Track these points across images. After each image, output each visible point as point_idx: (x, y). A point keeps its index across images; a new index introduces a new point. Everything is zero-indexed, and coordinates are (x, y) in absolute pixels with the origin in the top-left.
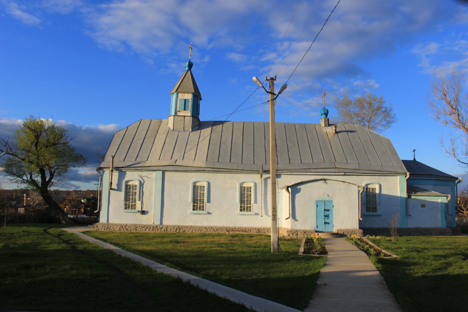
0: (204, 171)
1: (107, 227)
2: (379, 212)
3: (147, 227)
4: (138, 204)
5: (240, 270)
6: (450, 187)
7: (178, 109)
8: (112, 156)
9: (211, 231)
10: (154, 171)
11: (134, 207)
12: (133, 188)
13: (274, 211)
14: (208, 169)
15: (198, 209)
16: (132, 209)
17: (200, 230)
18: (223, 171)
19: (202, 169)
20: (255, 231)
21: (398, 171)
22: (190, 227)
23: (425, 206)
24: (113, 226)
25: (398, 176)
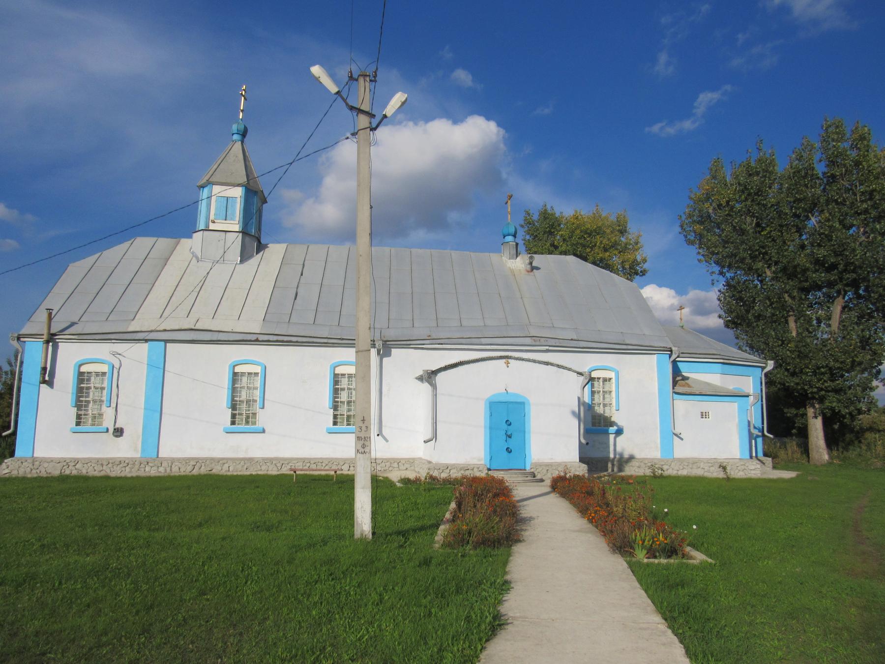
0: (257, 340)
1: (32, 468)
2: (259, 425)
3: (125, 465)
4: (108, 413)
7: (212, 217)
8: (47, 309)
9: (270, 469)
10: (146, 341)
11: (98, 417)
13: (364, 428)
14: (266, 338)
15: (244, 422)
16: (348, 425)
17: (245, 467)
19: (254, 337)
21: (656, 345)
22: (225, 461)
24: (46, 465)
25: (655, 354)
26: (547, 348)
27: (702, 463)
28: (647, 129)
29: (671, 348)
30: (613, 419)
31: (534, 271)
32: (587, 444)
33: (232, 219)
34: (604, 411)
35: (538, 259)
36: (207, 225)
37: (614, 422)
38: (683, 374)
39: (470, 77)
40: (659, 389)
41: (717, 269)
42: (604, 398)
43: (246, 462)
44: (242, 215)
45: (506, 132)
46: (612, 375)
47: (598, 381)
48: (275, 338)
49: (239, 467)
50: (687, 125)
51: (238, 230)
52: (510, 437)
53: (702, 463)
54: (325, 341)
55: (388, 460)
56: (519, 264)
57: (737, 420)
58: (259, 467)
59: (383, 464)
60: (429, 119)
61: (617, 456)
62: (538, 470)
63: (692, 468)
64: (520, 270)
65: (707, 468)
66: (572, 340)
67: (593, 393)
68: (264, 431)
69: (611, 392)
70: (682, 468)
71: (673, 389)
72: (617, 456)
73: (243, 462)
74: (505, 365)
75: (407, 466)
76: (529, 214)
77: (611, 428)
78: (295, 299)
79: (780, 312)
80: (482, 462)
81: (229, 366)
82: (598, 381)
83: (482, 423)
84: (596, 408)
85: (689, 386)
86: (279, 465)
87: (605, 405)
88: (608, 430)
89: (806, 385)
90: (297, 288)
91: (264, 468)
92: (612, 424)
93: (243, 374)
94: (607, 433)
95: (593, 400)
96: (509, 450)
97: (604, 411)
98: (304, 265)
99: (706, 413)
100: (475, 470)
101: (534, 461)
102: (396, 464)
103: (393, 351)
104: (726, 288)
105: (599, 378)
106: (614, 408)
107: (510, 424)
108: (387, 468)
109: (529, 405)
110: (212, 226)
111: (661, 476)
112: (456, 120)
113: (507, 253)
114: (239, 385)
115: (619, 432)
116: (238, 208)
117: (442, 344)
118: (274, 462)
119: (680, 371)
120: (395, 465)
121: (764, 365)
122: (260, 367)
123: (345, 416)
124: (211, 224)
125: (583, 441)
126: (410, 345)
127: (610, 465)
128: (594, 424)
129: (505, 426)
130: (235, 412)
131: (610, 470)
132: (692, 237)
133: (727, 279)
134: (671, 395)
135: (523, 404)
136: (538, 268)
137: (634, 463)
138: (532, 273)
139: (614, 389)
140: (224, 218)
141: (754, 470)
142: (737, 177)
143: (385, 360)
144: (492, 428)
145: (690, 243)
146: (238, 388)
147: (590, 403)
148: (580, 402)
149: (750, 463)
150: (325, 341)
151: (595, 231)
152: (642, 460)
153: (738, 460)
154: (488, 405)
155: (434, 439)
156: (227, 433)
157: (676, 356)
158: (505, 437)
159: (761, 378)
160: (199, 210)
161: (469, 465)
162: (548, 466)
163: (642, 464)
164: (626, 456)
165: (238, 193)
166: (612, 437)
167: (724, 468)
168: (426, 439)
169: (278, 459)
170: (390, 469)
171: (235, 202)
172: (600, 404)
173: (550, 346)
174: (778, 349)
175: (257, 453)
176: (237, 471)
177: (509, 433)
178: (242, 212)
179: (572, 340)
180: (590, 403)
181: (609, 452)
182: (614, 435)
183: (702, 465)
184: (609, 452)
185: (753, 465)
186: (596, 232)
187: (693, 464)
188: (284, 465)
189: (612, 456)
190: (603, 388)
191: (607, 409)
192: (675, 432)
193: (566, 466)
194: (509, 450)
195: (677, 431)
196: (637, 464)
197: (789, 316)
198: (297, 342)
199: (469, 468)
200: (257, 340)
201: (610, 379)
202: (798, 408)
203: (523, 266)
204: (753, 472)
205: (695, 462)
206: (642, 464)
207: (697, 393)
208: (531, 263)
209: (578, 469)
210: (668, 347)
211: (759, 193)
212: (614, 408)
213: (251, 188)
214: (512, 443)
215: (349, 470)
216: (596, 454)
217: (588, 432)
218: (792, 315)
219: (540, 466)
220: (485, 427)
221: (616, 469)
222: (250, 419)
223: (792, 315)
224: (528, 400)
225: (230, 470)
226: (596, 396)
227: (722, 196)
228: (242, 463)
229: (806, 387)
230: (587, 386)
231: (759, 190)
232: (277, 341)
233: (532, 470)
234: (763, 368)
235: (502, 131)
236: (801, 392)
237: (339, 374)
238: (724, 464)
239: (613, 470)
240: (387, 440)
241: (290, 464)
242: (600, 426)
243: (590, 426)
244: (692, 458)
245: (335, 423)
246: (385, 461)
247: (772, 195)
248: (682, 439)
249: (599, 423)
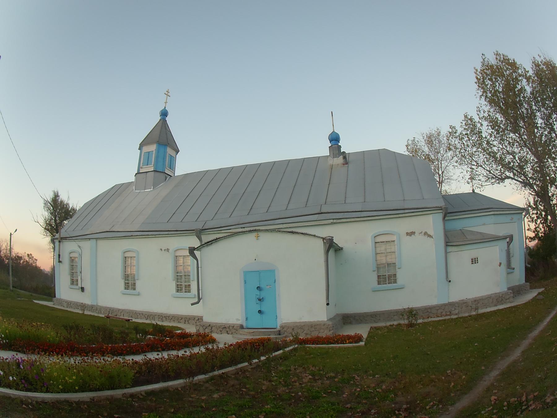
23: (477, 260)
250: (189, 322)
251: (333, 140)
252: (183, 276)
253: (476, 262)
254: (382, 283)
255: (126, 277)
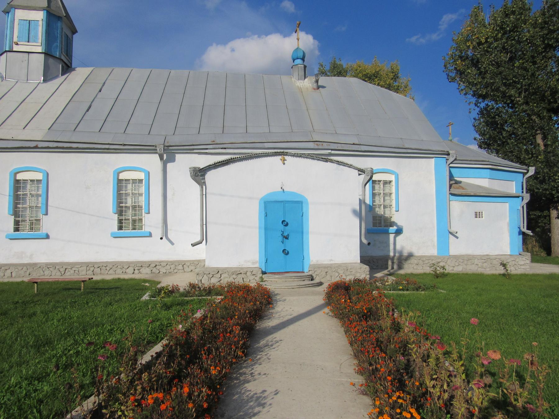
0: (36, 147)
5: (526, 120)
6: (514, 182)
7: (15, 40)
9: (53, 274)
12: (136, 226)
16: (134, 229)
17: (28, 273)
18: (79, 147)
19: (33, 144)
20: (148, 270)
21: (434, 149)
22: (6, 268)
23: (482, 215)
25: (433, 158)
26: (330, 151)
27: (476, 259)
28: (407, 40)
29: (448, 152)
30: (393, 220)
31: (320, 89)
32: (369, 244)
33: (34, 41)
34: (384, 212)
35: (323, 80)
36: (11, 47)
37: (394, 222)
38: (455, 179)
39: (293, 6)
40: (437, 191)
41: (474, 100)
42: (384, 200)
43: (28, 267)
44: (44, 37)
45: (319, 43)
46: (392, 178)
47: (379, 184)
48: (55, 145)
49: (22, 272)
50: (434, 37)
51: (41, 51)
52: (287, 238)
53: (476, 259)
54: (107, 147)
55: (172, 263)
56: (308, 83)
57: (508, 220)
58: (42, 272)
59: (168, 267)
60: (267, 34)
61: (397, 255)
62: (316, 273)
63: (466, 265)
64: (307, 88)
65: (480, 264)
66: (354, 144)
67: (374, 195)
68: (47, 237)
69: (391, 194)
70: (457, 264)
71: (450, 191)
72: (397, 255)
73: (25, 267)
74: (281, 162)
75: (192, 268)
76: (322, 66)
77: (391, 228)
78: (88, 110)
79: (529, 131)
80: (257, 265)
81: (11, 173)
82: (379, 184)
83: (257, 225)
84: (377, 209)
85: (463, 189)
86: (62, 270)
87: (385, 207)
88: (388, 230)
89: (554, 190)
90: (92, 102)
91: (47, 272)
92: (392, 224)
93: (25, 181)
94: (387, 233)
95: (374, 201)
96: (286, 252)
97: (384, 212)
98: (104, 83)
99: (479, 213)
100: (248, 274)
101: (312, 263)
102: (181, 266)
103: (178, 156)
104: (480, 116)
105: (380, 181)
106: (394, 209)
107: (287, 225)
108: (172, 270)
109: (307, 204)
110: (16, 48)
111: (444, 275)
112: (286, 35)
113: (296, 74)
114: (21, 193)
115: (399, 232)
116: (40, 31)
117: (225, 148)
118: (57, 267)
119: (453, 177)
120: (180, 267)
121: (526, 171)
122: (42, 174)
123: (131, 221)
124: (14, 46)
125: (365, 241)
126: (194, 149)
127: (390, 263)
128: (374, 225)
129: (282, 227)
130: (17, 219)
131: (390, 268)
132: (453, 75)
133: (481, 109)
134: (448, 196)
135: (300, 203)
136: (323, 87)
137: (412, 261)
138: (318, 91)
139: (393, 190)
140: (27, 40)
141: (523, 265)
142: (495, 18)
143: (169, 165)
144: (267, 229)
145: (453, 80)
146: (20, 195)
147: (372, 205)
148: (362, 202)
149: (521, 259)
150: (107, 147)
151: (374, 75)
152: (420, 258)
153: (508, 256)
154: (263, 205)
155: (204, 241)
156: (11, 239)
157: (454, 159)
158: (281, 238)
159: (522, 182)
160: (5, 34)
161: (242, 268)
162: (328, 268)
163: (421, 262)
164: (405, 254)
165: (39, 16)
166: (392, 237)
167: (504, 265)
168: (194, 242)
169: (62, 264)
170: (175, 271)
171: (37, 25)
172: (381, 205)
173: (332, 150)
174: (529, 160)
175: (42, 259)
176: (19, 277)
177: (285, 234)
178: (44, 35)
179: (354, 144)
180: (372, 205)
181: (389, 251)
182: (394, 234)
183: (476, 261)
184: (389, 251)
185: (523, 260)
186: (375, 76)
187: (469, 260)
188: (67, 270)
189: (392, 254)
190: (384, 191)
191: (387, 210)
192: (451, 231)
193: (346, 267)
194: (286, 252)
195: (453, 230)
196: (416, 262)
197: (537, 134)
198: (77, 148)
199: (241, 272)
200: (36, 147)
201: (390, 182)
202: (542, 211)
203: (310, 85)
204: (523, 267)
205: (469, 258)
206: (421, 262)
207: (472, 194)
208: (317, 81)
209: (359, 271)
210: (446, 150)
211: (515, 28)
212: (394, 209)
213: (51, 12)
214: (289, 245)
215: (133, 273)
216: (376, 253)
217: (369, 232)
218: (539, 133)
219: (319, 268)
220: (260, 228)
221: (395, 267)
222: (35, 224)
223: (539, 133)
224: (307, 199)
225: (13, 276)
226: (377, 198)
227: (482, 35)
228: (25, 268)
229: (554, 192)
230: (368, 184)
231: (516, 27)
232: (57, 148)
233: (310, 273)
234: (524, 174)
235: (316, 42)
236: (548, 197)
237: (123, 180)
238: (505, 263)
239: (393, 268)
240: (172, 244)
241: (74, 269)
242: (380, 226)
243: (371, 226)
244: (467, 255)
245: (120, 228)
246: (170, 264)
247: (527, 32)
248: (457, 238)
249: (380, 223)
250: (141, 270)
251: (298, 59)
252: (131, 207)
253: (481, 216)
254: (133, 212)
255: (120, 211)
